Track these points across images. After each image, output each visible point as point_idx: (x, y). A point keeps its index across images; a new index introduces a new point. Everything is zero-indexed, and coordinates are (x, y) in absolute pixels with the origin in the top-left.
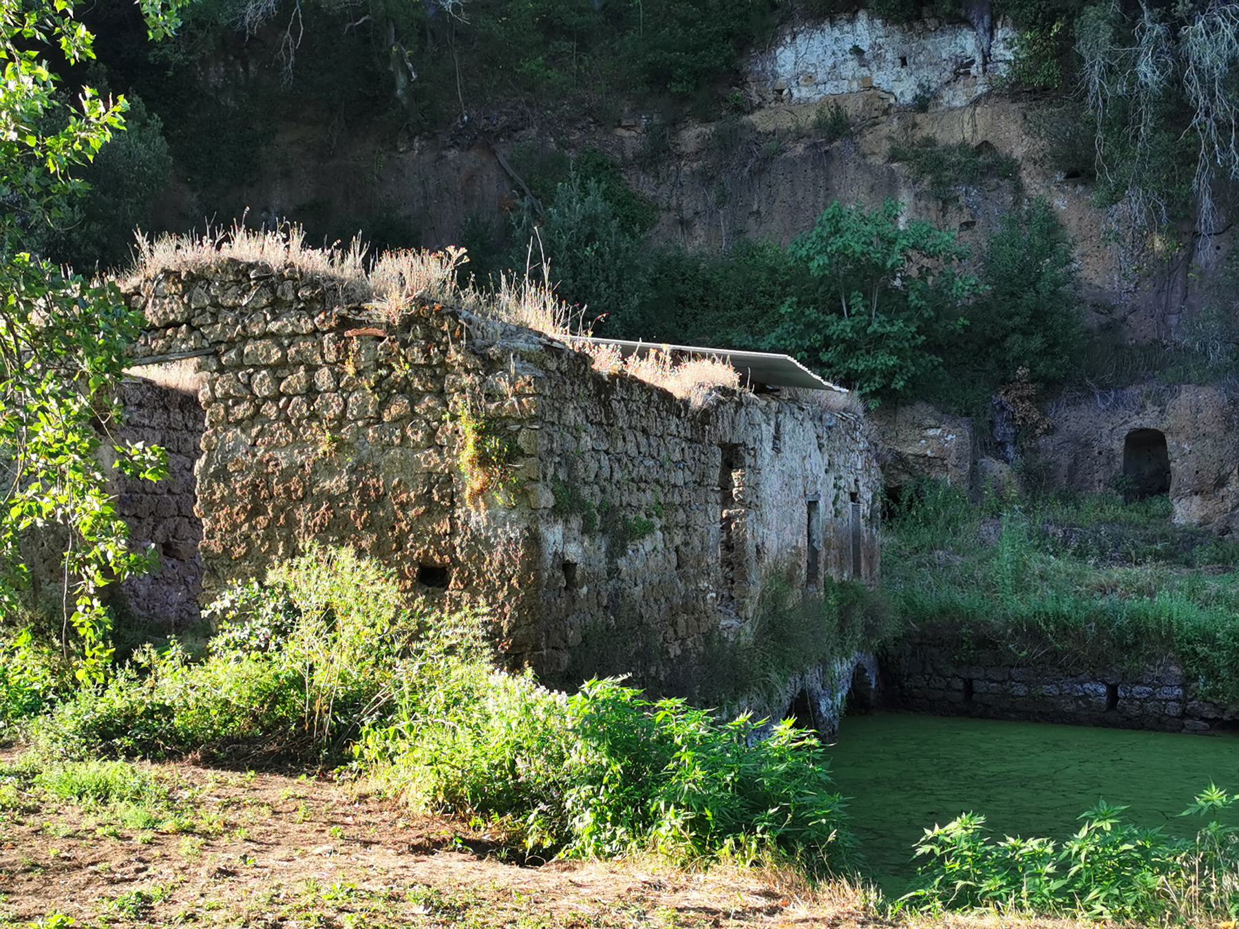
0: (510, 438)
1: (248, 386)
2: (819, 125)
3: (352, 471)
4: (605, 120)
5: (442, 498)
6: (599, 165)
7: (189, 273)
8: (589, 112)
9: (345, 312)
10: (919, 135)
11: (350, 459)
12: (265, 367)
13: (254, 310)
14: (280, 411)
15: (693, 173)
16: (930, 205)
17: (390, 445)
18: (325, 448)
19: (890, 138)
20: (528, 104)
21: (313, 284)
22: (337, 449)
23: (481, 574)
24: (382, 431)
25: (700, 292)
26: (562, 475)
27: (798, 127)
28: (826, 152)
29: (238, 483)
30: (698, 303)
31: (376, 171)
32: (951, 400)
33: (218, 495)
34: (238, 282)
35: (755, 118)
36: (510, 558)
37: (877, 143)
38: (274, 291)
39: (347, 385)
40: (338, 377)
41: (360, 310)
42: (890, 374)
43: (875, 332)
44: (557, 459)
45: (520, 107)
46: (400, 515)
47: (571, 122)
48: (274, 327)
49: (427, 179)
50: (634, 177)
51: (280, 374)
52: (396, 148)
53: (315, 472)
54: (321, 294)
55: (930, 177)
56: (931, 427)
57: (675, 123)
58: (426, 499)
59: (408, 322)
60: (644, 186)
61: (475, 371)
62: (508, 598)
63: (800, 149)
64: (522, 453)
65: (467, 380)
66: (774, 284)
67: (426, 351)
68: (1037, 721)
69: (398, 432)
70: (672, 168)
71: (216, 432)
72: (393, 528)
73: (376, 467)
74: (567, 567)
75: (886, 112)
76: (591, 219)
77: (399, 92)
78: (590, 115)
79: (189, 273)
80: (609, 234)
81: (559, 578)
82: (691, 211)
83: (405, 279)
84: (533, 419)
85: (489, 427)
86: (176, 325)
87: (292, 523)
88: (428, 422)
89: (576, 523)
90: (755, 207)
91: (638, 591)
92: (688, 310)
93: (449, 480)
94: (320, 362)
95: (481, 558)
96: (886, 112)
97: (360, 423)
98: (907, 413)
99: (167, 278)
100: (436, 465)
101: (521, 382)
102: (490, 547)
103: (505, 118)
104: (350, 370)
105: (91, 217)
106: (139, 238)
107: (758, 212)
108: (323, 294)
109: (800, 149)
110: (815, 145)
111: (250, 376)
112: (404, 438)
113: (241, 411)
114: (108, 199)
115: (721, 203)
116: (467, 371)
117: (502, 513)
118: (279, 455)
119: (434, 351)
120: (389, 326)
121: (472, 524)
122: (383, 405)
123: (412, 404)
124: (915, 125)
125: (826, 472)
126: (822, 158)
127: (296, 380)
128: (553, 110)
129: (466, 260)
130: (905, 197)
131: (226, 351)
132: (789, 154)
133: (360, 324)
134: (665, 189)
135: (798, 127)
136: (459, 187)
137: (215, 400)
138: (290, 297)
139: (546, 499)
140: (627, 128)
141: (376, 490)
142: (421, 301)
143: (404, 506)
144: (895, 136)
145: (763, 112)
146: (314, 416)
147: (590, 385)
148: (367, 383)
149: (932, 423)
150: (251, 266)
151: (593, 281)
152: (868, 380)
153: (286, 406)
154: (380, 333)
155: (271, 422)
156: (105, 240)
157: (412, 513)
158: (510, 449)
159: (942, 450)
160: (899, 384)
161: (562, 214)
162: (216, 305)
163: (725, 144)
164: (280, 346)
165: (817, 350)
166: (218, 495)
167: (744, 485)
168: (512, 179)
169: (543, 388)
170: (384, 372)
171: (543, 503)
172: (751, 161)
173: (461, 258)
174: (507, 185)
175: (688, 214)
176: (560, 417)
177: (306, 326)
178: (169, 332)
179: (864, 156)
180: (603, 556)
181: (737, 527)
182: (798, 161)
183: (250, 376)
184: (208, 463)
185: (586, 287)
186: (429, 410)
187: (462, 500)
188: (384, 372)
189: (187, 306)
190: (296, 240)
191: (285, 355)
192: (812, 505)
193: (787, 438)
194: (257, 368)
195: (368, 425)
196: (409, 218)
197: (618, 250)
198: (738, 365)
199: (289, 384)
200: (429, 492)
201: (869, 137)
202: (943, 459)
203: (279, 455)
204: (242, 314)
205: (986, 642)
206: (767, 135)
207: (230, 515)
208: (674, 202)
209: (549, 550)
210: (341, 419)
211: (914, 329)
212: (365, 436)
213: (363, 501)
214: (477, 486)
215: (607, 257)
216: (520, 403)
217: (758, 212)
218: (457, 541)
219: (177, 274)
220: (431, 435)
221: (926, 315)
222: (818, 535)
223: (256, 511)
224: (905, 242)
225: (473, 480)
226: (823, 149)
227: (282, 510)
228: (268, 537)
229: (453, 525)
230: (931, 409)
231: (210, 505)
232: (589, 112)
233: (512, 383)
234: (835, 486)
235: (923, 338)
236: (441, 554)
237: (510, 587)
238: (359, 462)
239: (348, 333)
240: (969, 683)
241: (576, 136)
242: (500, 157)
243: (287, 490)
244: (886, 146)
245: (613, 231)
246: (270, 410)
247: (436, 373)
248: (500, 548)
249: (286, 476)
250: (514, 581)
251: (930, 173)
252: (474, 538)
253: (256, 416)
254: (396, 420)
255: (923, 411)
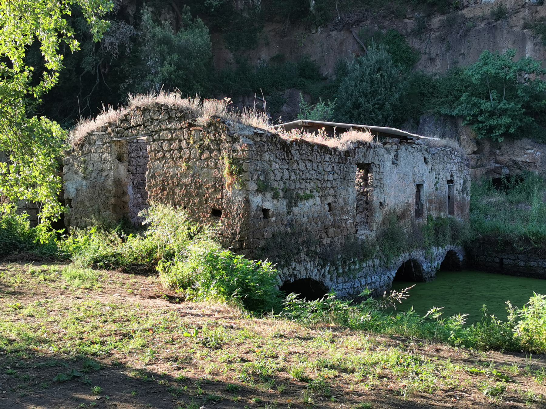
0: (240, 165)
1: (161, 146)
2: (493, 13)
3: (192, 176)
4: (400, 16)
5: (219, 186)
6: (395, 36)
7: (144, 108)
8: (393, 12)
9: (190, 121)
10: (538, 16)
11: (191, 172)
12: (167, 140)
13: (164, 121)
14: (171, 155)
15: (436, 37)
16: (541, 49)
17: (204, 167)
18: (183, 168)
19: (524, 19)
20: (367, 10)
21: (181, 112)
22: (188, 169)
23: (231, 212)
24: (201, 163)
25: (431, 90)
26: (262, 178)
27: (484, 15)
28: (494, 26)
29: (159, 179)
30: (430, 95)
31: (303, 42)
32: (540, 137)
33: (152, 184)
34: (159, 111)
35: (464, 12)
36: (239, 207)
37: (517, 21)
38: (169, 114)
39: (191, 146)
40: (188, 144)
41: (195, 121)
42: (508, 126)
43: (501, 108)
44: (260, 173)
45: (363, 12)
46: (206, 191)
47: (384, 17)
48: (169, 126)
49: (323, 44)
50: (411, 40)
51: (171, 143)
52: (311, 32)
53: (181, 176)
54: (184, 115)
55: (541, 36)
56: (529, 149)
57: (429, 16)
58: (214, 186)
59: (210, 125)
60: (415, 43)
61: (229, 142)
62: (239, 221)
63: (483, 25)
64: (244, 171)
65: (227, 145)
66: (462, 86)
67: (214, 135)
68: (528, 277)
69: (206, 163)
70: (427, 35)
71: (152, 162)
72: (204, 196)
73: (199, 175)
74: (265, 212)
75: (523, 6)
76: (380, 62)
77: (311, 9)
78: (393, 13)
79: (144, 108)
80: (388, 67)
81: (260, 215)
82: (435, 54)
83: (211, 108)
84: (248, 159)
85: (234, 161)
86: (140, 125)
87: (174, 193)
88: (215, 160)
89: (269, 195)
90: (462, 52)
91: (305, 219)
92: (426, 98)
93: (221, 180)
94: (183, 139)
95: (231, 207)
96: (523, 6)
97: (195, 160)
98: (518, 143)
99: (137, 109)
100: (217, 175)
101: (243, 146)
102: (233, 203)
103: (356, 17)
104: (192, 141)
105: (179, 68)
106: (129, 95)
107: (464, 54)
108: (184, 115)
109: (483, 25)
110: (489, 23)
111: (162, 143)
112: (208, 165)
113: (159, 155)
114: (186, 61)
115: (448, 50)
116: (227, 142)
117: (237, 192)
118: (171, 170)
119: (217, 135)
120: (204, 126)
121: (228, 195)
122: (202, 154)
123: (210, 153)
124: (537, 12)
125: (429, 172)
126: (492, 28)
127: (175, 145)
128: (377, 12)
129: (232, 102)
130: (529, 46)
131: (155, 134)
132: (477, 28)
133: (195, 125)
134: (424, 45)
135: (484, 15)
136: (336, 47)
137: (152, 151)
138: (174, 116)
139: (253, 186)
140: (409, 19)
141: (199, 183)
142: (214, 117)
143: (207, 189)
144: (526, 17)
145: (468, 9)
146: (181, 157)
147: (279, 146)
148: (197, 146)
149: (530, 147)
150: (162, 105)
151: (379, 87)
152: (499, 130)
153: (172, 154)
154: (201, 129)
155: (168, 159)
156: (185, 77)
157: (210, 191)
158: (240, 169)
159: (534, 159)
160: (512, 130)
161: (368, 60)
162: (152, 119)
163: (450, 24)
164: (171, 133)
165: (477, 116)
166: (152, 184)
167: (373, 179)
168: (359, 43)
169: (252, 148)
170: (202, 142)
171: (251, 188)
172: (461, 31)
173: (230, 102)
174: (356, 46)
175: (433, 55)
176: (261, 157)
177: (179, 126)
178: (138, 128)
179: (511, 27)
180: (285, 207)
181: (370, 195)
182: (481, 30)
183: (162, 143)
184: (149, 173)
185: (376, 90)
186: (216, 155)
187: (225, 187)
188: (202, 142)
189: (143, 119)
190: (179, 96)
191: (172, 136)
192: (419, 187)
193: (402, 159)
194: (164, 140)
195: (197, 160)
196: (315, 61)
197: (391, 74)
198: (373, 132)
199: (174, 146)
200: (215, 184)
201: (514, 18)
202: (535, 163)
203: (171, 170)
204: (160, 122)
205: (508, 243)
206: (470, 19)
207: (156, 190)
208: (427, 51)
209: (254, 206)
210: (189, 159)
211: (520, 106)
212: (196, 164)
213: (195, 187)
214: (230, 182)
215: (386, 77)
216: (243, 153)
217: (464, 54)
218: (223, 201)
219: (140, 108)
220: (216, 164)
221: (526, 100)
222: (424, 198)
223: (164, 189)
224: (515, 68)
225: (228, 180)
226: (493, 25)
227: (171, 189)
228: (167, 198)
229: (222, 196)
230: (529, 141)
231: (150, 187)
232: (393, 12)
233: (241, 146)
234: (436, 178)
235: (524, 110)
236: (219, 205)
237: (240, 217)
238: (194, 173)
239: (191, 129)
240: (501, 260)
241: (386, 23)
242: (354, 34)
243: (173, 182)
244: (522, 22)
245: (389, 66)
246: (168, 155)
247: (218, 142)
248: (236, 204)
249: (172, 177)
250: (241, 215)
251: (541, 33)
252: (229, 200)
253: (164, 157)
254: (206, 159)
255: (525, 142)
